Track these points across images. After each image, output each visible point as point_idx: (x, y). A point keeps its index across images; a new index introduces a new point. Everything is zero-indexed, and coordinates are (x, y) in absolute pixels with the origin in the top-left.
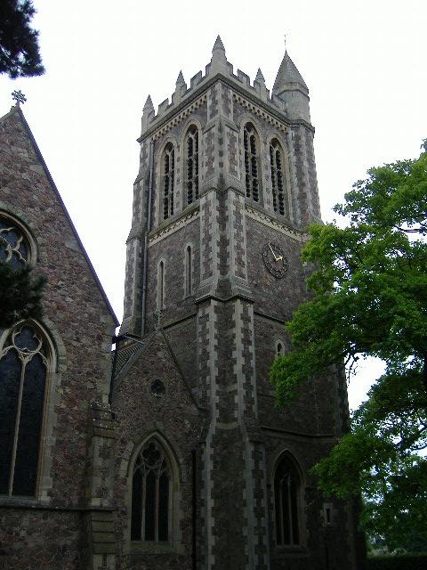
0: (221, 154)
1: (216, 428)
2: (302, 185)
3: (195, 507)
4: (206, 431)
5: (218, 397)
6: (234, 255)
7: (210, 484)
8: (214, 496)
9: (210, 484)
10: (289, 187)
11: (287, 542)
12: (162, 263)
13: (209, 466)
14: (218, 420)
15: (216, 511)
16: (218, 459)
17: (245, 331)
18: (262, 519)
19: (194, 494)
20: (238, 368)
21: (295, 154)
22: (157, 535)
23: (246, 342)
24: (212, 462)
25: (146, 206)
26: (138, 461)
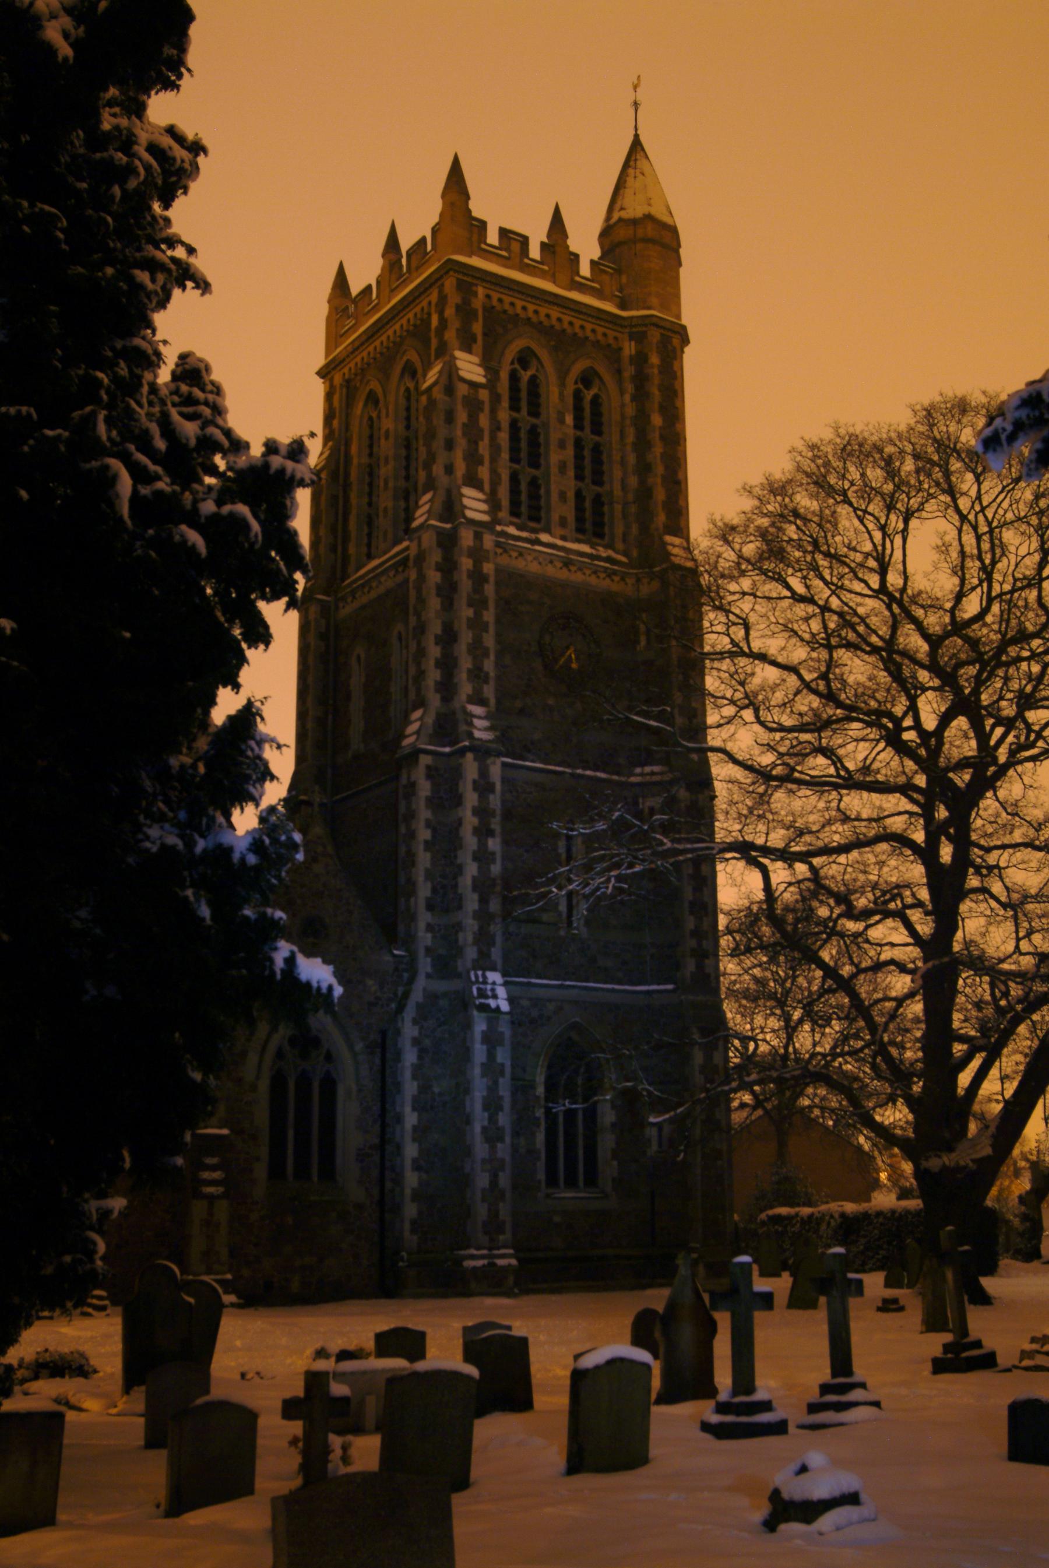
0: (450, 445)
1: (424, 990)
2: (644, 468)
3: (384, 1126)
4: (406, 995)
5: (429, 935)
6: (466, 663)
7: (410, 1088)
8: (418, 1106)
9: (410, 1088)
10: (617, 474)
11: (571, 1182)
12: (359, 657)
13: (410, 1057)
14: (428, 976)
15: (420, 1133)
16: (427, 1042)
17: (483, 812)
18: (499, 1145)
19: (383, 1102)
20: (466, 881)
21: (634, 399)
22: (315, 1171)
23: (483, 832)
24: (415, 1050)
25: (333, 530)
26: (280, 1054)
